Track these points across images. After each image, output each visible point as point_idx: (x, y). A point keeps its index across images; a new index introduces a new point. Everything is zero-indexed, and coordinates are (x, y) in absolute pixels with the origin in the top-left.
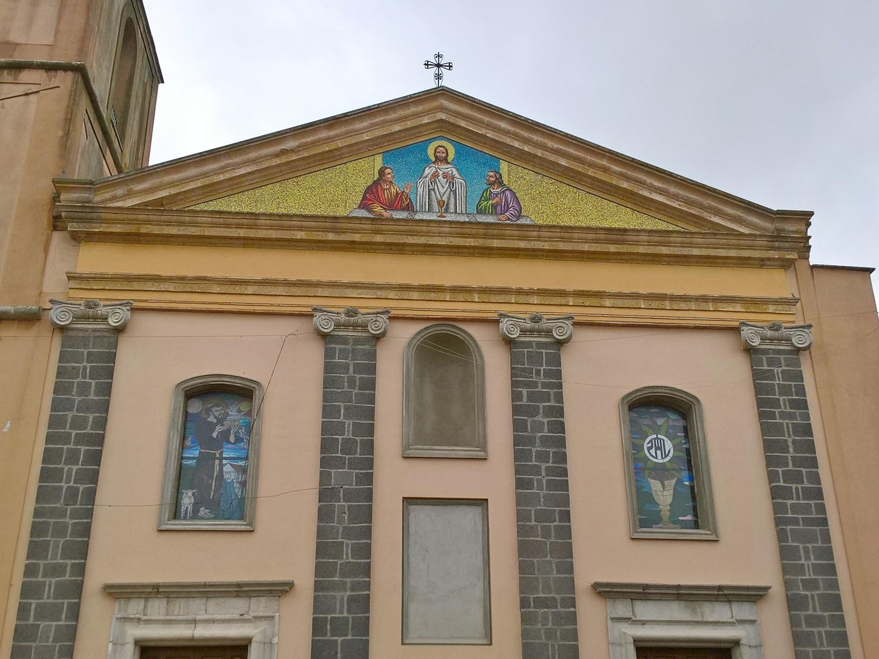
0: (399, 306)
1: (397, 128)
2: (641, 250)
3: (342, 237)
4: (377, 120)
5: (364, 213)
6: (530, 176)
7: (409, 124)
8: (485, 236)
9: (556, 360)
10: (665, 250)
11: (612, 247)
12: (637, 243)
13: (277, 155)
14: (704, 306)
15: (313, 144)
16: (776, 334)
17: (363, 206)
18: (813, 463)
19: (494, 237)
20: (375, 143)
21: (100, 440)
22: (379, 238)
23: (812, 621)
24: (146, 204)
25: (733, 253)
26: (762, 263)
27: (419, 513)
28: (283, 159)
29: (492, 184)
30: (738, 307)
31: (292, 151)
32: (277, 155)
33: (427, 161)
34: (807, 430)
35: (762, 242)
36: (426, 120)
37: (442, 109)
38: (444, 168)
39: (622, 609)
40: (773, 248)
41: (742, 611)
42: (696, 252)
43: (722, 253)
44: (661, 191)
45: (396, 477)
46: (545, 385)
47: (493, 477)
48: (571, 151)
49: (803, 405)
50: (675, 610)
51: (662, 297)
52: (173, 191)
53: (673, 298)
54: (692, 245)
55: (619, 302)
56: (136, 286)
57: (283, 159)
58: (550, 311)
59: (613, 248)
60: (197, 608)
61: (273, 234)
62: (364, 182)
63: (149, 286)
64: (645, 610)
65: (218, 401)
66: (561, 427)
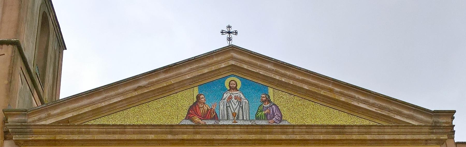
1: (206, 71)
2: (354, 137)
3: (176, 137)
5: (188, 122)
6: (286, 96)
7: (213, 68)
10: (368, 137)
12: (351, 133)
13: (135, 90)
15: (157, 82)
17: (188, 117)
20: (194, 80)
24: (59, 122)
28: (140, 92)
29: (264, 102)
31: (144, 87)
32: (135, 90)
33: (225, 90)
36: (223, 65)
37: (233, 58)
38: (235, 93)
40: (432, 133)
42: (387, 137)
48: (310, 80)
52: (75, 114)
54: (385, 133)
57: (140, 92)
59: (337, 137)
61: (135, 137)
62: (188, 104)
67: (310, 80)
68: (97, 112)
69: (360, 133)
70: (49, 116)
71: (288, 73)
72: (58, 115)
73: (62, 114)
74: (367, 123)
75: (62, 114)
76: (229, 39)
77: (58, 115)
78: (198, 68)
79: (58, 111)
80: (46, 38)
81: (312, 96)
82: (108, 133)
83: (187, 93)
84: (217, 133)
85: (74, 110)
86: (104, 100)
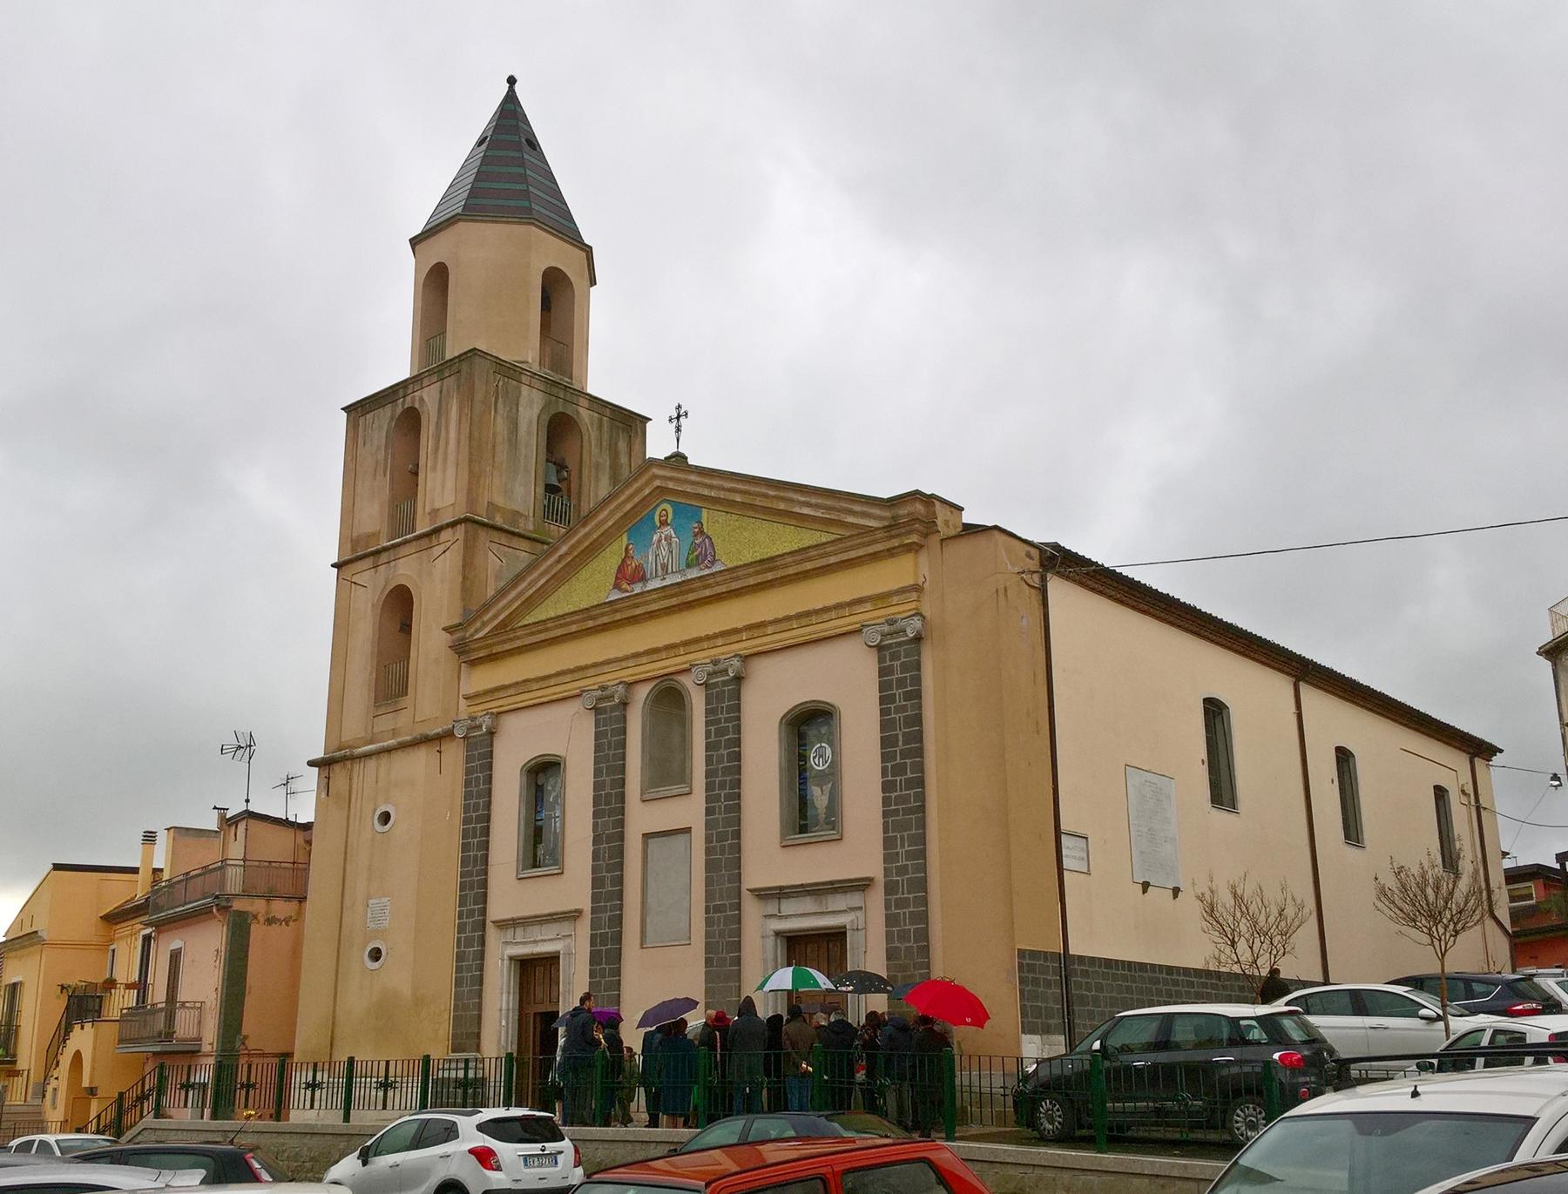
0: (627, 675)
1: (629, 507)
2: (791, 571)
3: (599, 622)
4: (612, 507)
5: (616, 595)
6: (721, 517)
7: (637, 500)
8: (682, 593)
9: (737, 695)
10: (808, 566)
11: (769, 574)
12: (786, 566)
13: (558, 561)
14: (841, 612)
15: (579, 542)
16: (893, 628)
17: (617, 586)
18: (920, 752)
19: (688, 592)
20: (618, 526)
21: (488, 818)
22: (618, 616)
23: (901, 903)
24: (496, 628)
25: (861, 552)
26: (891, 553)
27: (654, 844)
28: (563, 563)
29: (696, 535)
30: (869, 606)
31: (566, 554)
32: (558, 561)
33: (654, 529)
34: (917, 720)
35: (880, 535)
36: (647, 491)
37: (655, 477)
38: (668, 531)
39: (771, 908)
40: (893, 537)
41: (854, 899)
42: (833, 560)
43: (853, 554)
44: (808, 505)
45: (641, 818)
46: (727, 720)
47: (690, 811)
48: (740, 486)
49: (916, 695)
50: (808, 904)
51: (808, 614)
52: (507, 613)
53: (817, 612)
54: (829, 555)
55: (779, 627)
56: (497, 695)
57: (563, 563)
58: (721, 651)
59: (770, 576)
60: (536, 932)
61: (559, 632)
62: (615, 562)
63: (502, 694)
64: (789, 907)
65: (542, 772)
66: (738, 757)
67: (740, 486)
68: (530, 603)
69: (797, 563)
70: (484, 624)
71: (715, 482)
72: (492, 619)
73: (495, 616)
74: (825, 538)
75: (495, 616)
76: (129, 986)
77: (492, 619)
78: (618, 507)
79: (490, 615)
80: (250, 1025)
81: (747, 508)
82: (533, 634)
83: (615, 546)
84: (636, 606)
85: (504, 608)
86: (530, 585)
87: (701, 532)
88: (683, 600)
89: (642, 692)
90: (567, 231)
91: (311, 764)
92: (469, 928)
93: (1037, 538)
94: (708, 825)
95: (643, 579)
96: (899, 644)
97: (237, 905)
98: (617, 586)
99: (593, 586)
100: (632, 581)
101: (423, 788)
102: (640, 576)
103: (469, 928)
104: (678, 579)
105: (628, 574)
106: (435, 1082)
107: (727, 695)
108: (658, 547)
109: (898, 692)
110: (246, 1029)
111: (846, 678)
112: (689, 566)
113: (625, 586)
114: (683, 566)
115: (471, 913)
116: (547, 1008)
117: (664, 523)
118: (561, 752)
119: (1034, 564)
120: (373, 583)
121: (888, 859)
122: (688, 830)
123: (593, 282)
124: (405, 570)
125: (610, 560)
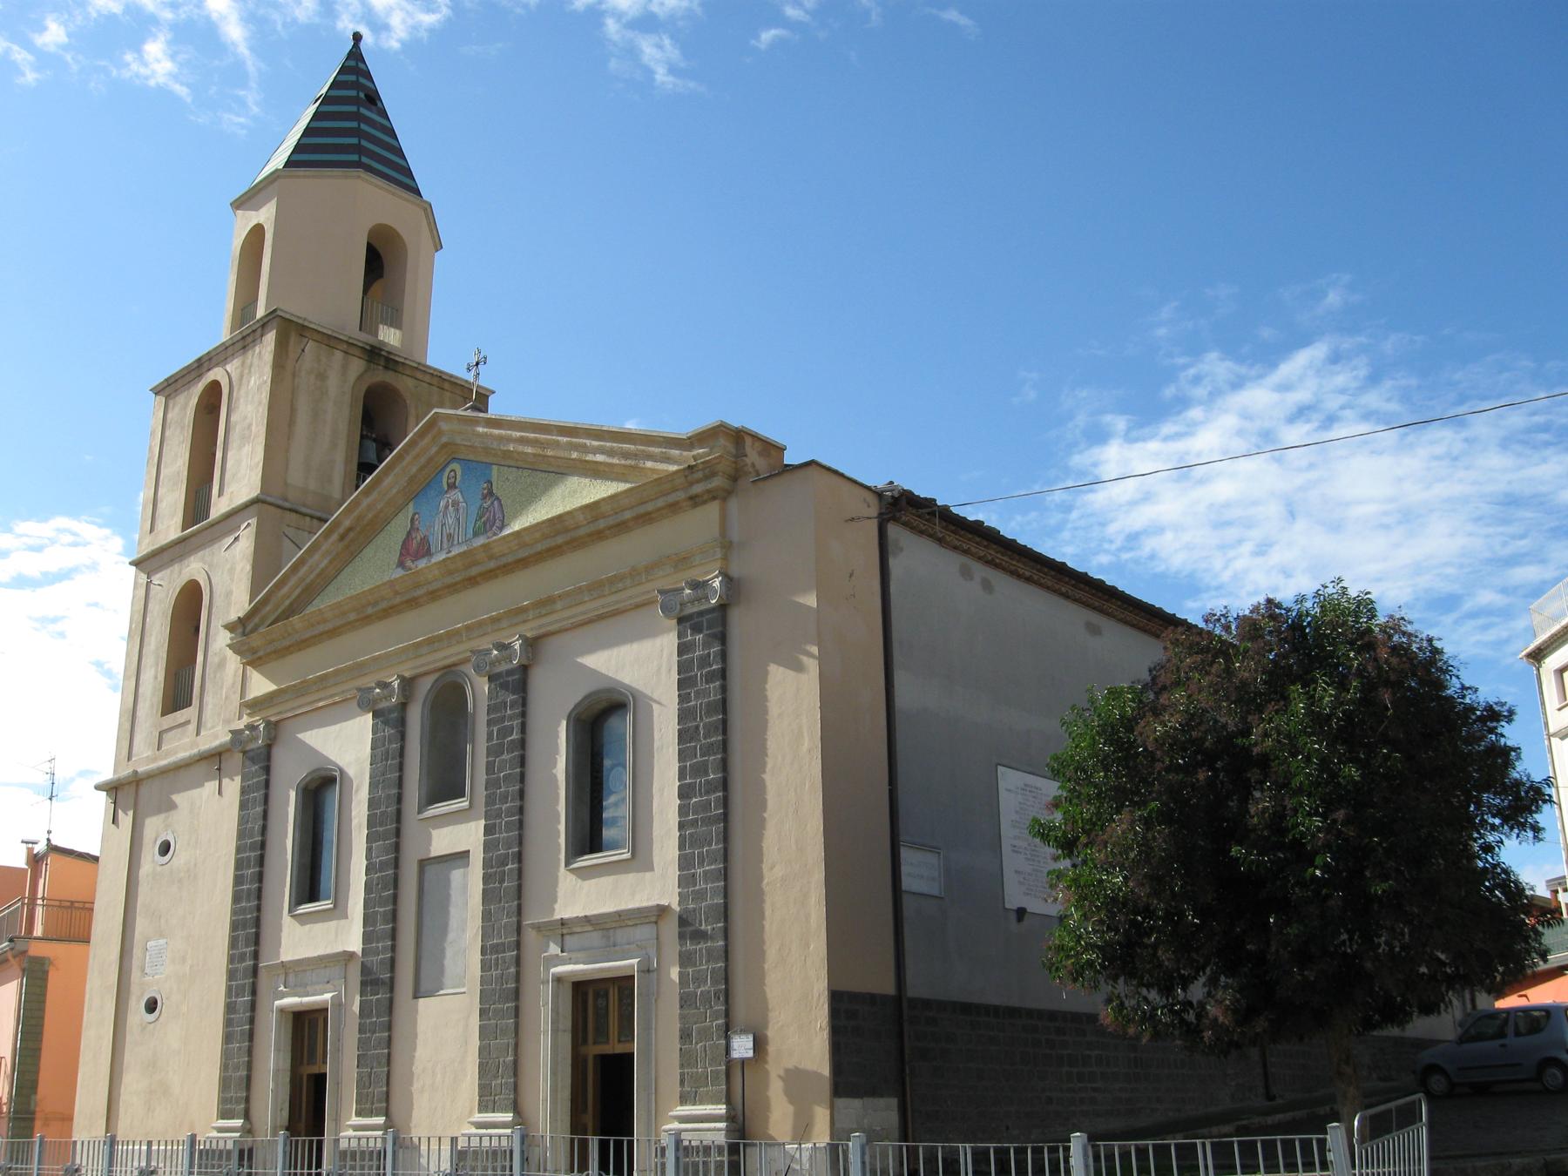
17: (401, 564)
33: (443, 493)
38: (456, 495)
87: (491, 493)
88: (474, 573)
89: (425, 685)
90: (400, 175)
91: (98, 788)
92: (240, 975)
93: (879, 482)
94: (487, 847)
95: (428, 553)
96: (701, 614)
97: (36, 949)
98: (401, 564)
99: (375, 569)
100: (417, 556)
101: (210, 816)
102: (425, 550)
103: (240, 975)
104: (464, 548)
105: (415, 548)
106: (201, 1151)
107: (516, 684)
108: (445, 515)
109: (698, 673)
110: (43, 1089)
111: (645, 664)
112: (476, 534)
113: (409, 563)
114: (470, 534)
115: (242, 958)
116: (315, 1070)
117: (452, 486)
118: (1509, 700)
119: (873, 511)
120: (168, 584)
121: (682, 882)
122: (465, 855)
123: (438, 246)
124: (193, 568)
125: (396, 531)
